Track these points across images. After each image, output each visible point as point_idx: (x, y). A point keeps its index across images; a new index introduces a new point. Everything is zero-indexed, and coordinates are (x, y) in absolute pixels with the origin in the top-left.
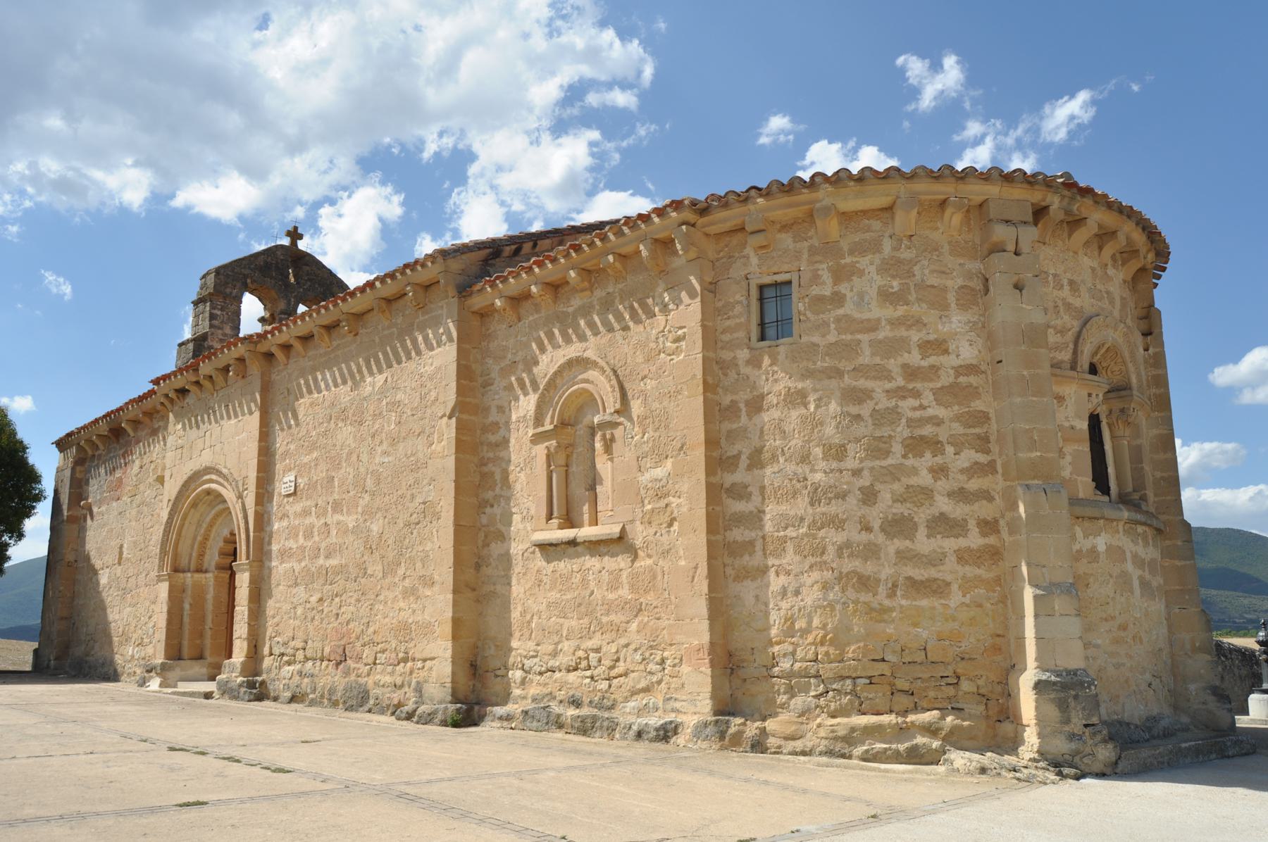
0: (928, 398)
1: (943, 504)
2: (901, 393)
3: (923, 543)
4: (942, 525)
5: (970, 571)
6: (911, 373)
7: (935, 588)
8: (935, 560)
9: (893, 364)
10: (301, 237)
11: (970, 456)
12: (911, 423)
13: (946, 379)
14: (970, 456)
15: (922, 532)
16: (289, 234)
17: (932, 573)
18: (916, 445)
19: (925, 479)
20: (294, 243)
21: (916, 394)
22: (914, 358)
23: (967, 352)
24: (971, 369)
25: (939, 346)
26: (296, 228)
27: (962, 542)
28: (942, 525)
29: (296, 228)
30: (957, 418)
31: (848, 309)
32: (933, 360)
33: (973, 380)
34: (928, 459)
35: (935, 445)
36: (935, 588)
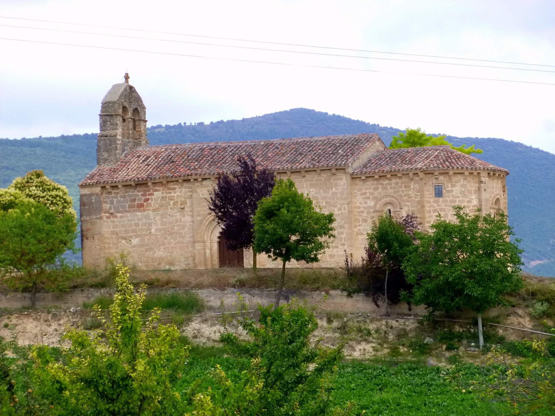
25: (469, 202)
26: (127, 74)
29: (127, 74)
31: (454, 193)
32: (469, 204)
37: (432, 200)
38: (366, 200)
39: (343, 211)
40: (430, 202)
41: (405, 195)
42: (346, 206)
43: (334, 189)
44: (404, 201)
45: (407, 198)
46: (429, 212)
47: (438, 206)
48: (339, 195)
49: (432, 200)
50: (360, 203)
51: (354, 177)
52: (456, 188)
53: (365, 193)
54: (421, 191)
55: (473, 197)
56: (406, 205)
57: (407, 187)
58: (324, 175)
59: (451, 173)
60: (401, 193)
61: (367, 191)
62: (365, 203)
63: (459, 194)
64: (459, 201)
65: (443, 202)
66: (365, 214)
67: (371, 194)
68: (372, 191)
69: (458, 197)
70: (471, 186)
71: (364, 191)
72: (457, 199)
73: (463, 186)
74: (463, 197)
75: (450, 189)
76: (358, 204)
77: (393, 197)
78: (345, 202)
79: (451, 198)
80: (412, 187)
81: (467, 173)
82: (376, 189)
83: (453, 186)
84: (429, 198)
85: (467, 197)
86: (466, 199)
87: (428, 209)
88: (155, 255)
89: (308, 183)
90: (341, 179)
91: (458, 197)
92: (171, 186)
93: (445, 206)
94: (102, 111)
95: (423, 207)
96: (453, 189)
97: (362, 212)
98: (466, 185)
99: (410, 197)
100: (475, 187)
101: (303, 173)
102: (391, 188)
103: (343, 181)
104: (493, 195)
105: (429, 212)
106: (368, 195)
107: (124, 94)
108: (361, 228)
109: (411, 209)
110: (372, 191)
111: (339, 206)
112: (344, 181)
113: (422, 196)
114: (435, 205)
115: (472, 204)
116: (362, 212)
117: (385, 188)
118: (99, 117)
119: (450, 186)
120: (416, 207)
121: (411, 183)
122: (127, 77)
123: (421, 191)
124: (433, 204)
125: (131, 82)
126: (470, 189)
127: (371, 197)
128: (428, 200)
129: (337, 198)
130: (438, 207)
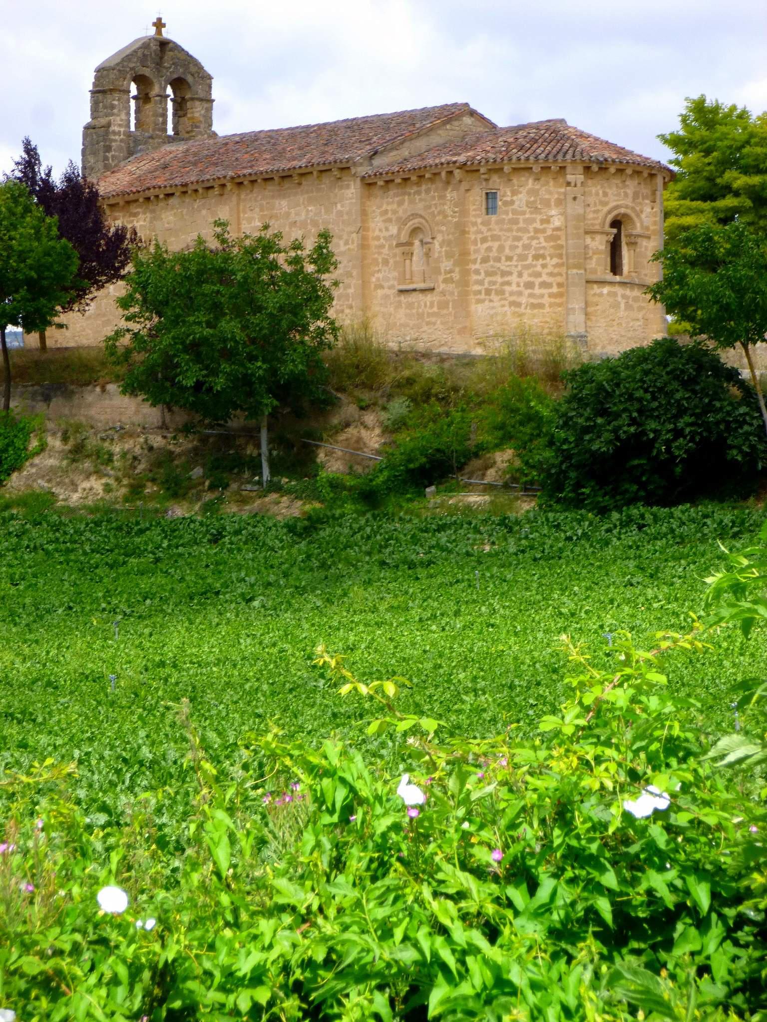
0: (542, 240)
1: (545, 278)
2: (532, 238)
3: (537, 291)
4: (544, 285)
5: (553, 300)
6: (537, 231)
7: (541, 306)
8: (542, 296)
9: (531, 228)
10: (164, 25)
11: (555, 261)
12: (536, 249)
13: (549, 232)
14: (555, 261)
15: (537, 287)
16: (154, 24)
17: (540, 301)
18: (536, 257)
19: (539, 269)
20: (159, 32)
21: (538, 238)
22: (538, 225)
23: (557, 222)
24: (558, 229)
25: (547, 221)
26: (159, 19)
27: (550, 291)
28: (544, 285)
29: (159, 19)
30: (552, 247)
31: (515, 206)
32: (545, 226)
33: (559, 233)
34: (541, 262)
35: (543, 257)
36: (541, 306)
37: (479, 220)
38: (387, 224)
39: (351, 246)
40: (475, 224)
41: (439, 213)
42: (354, 235)
43: (339, 206)
44: (437, 224)
45: (441, 217)
46: (475, 242)
47: (489, 230)
48: (345, 217)
49: (479, 220)
50: (380, 230)
51: (368, 184)
52: (520, 196)
53: (386, 212)
54: (461, 204)
55: (553, 212)
56: (440, 231)
57: (442, 197)
58: (327, 180)
59: (507, 169)
60: (433, 209)
61: (389, 208)
62: (387, 229)
63: (525, 208)
64: (525, 221)
65: (497, 223)
66: (385, 251)
67: (395, 212)
68: (395, 206)
69: (524, 213)
70: (551, 193)
71: (384, 207)
72: (521, 217)
73: (531, 192)
74: (531, 213)
75: (509, 199)
76: (377, 233)
77: (421, 216)
78: (353, 229)
79: (510, 216)
80: (449, 196)
81: (536, 169)
82: (400, 204)
83: (514, 193)
84: (475, 216)
85: (541, 213)
86: (539, 217)
87: (473, 237)
88: (472, 296)
89: (306, 196)
90: (348, 187)
91: (524, 213)
92: (134, 209)
93: (501, 230)
94: (95, 85)
95: (464, 232)
96: (515, 198)
97: (382, 246)
98: (538, 190)
99: (446, 216)
100: (558, 193)
101: (296, 179)
102: (421, 200)
103: (352, 191)
104: (606, 209)
105: (475, 242)
106: (389, 215)
107: (140, 54)
108: (380, 275)
109: (446, 237)
110: (395, 206)
111: (345, 237)
112: (352, 190)
113: (464, 213)
114: (484, 229)
115: (552, 226)
116: (382, 246)
117: (412, 202)
118: (89, 95)
119: (509, 193)
120: (453, 234)
121: (446, 189)
122: (159, 24)
123: (461, 204)
124: (480, 227)
125: (166, 34)
126: (547, 197)
127: (394, 218)
128: (474, 220)
129: (343, 222)
130: (489, 234)
